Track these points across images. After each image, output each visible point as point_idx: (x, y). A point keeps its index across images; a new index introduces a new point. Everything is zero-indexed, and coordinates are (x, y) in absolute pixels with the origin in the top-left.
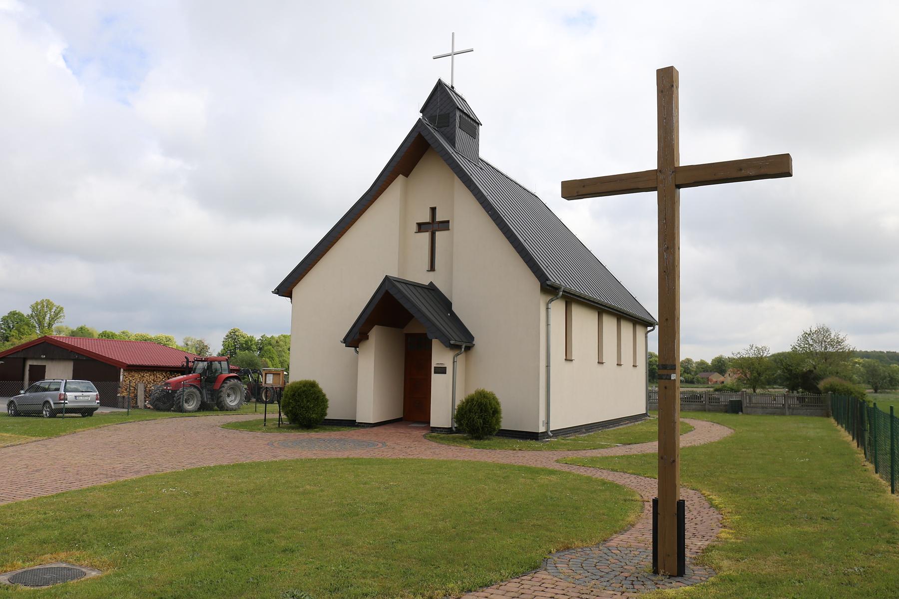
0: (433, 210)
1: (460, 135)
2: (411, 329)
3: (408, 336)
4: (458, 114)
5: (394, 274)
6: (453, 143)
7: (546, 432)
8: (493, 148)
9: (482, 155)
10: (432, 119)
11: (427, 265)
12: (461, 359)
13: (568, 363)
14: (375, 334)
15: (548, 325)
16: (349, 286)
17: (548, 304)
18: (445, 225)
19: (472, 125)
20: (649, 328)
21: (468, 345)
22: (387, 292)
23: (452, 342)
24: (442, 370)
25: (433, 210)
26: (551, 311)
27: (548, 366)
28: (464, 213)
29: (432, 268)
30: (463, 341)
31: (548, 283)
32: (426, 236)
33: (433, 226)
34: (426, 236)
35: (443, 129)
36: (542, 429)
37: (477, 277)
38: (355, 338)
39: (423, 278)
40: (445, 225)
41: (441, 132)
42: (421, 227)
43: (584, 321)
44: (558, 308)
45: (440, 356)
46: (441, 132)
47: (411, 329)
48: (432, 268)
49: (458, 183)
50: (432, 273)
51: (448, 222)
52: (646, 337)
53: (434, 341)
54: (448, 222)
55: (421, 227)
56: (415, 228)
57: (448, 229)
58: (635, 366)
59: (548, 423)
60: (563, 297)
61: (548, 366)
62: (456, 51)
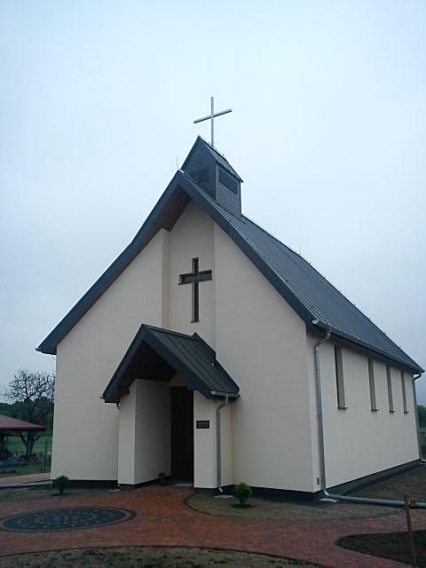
0: (196, 261)
1: (220, 189)
2: (174, 383)
3: (173, 388)
4: (217, 167)
5: (156, 323)
6: (214, 197)
7: (322, 491)
8: (255, 205)
9: (244, 212)
10: (192, 175)
11: (190, 317)
12: (225, 412)
13: (342, 411)
14: (135, 387)
15: (316, 370)
16: (108, 342)
17: (315, 348)
18: (208, 275)
19: (233, 182)
20: (415, 376)
21: (233, 395)
22: (143, 342)
23: (213, 393)
24: (204, 425)
25: (196, 261)
26: (320, 356)
27: (320, 416)
28: (227, 264)
29: (196, 319)
30: (227, 393)
31: (315, 322)
32: (190, 287)
33: (196, 277)
34: (190, 287)
35: (202, 184)
36: (316, 488)
37: (243, 328)
38: (115, 393)
39: (189, 330)
40: (208, 275)
41: (200, 193)
42: (184, 279)
43: (355, 368)
44: (327, 356)
45: (202, 410)
46: (200, 193)
47: (174, 383)
48: (196, 319)
49: (218, 230)
50: (196, 324)
51: (210, 272)
52: (414, 384)
53: (196, 393)
54: (210, 272)
55: (184, 279)
56: (178, 280)
57: (211, 279)
58: (405, 413)
59: (322, 480)
60: (330, 341)
61: (320, 416)
62: (215, 112)
